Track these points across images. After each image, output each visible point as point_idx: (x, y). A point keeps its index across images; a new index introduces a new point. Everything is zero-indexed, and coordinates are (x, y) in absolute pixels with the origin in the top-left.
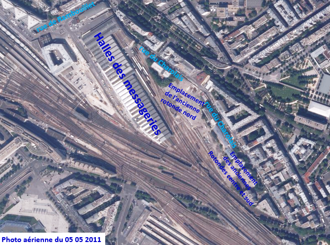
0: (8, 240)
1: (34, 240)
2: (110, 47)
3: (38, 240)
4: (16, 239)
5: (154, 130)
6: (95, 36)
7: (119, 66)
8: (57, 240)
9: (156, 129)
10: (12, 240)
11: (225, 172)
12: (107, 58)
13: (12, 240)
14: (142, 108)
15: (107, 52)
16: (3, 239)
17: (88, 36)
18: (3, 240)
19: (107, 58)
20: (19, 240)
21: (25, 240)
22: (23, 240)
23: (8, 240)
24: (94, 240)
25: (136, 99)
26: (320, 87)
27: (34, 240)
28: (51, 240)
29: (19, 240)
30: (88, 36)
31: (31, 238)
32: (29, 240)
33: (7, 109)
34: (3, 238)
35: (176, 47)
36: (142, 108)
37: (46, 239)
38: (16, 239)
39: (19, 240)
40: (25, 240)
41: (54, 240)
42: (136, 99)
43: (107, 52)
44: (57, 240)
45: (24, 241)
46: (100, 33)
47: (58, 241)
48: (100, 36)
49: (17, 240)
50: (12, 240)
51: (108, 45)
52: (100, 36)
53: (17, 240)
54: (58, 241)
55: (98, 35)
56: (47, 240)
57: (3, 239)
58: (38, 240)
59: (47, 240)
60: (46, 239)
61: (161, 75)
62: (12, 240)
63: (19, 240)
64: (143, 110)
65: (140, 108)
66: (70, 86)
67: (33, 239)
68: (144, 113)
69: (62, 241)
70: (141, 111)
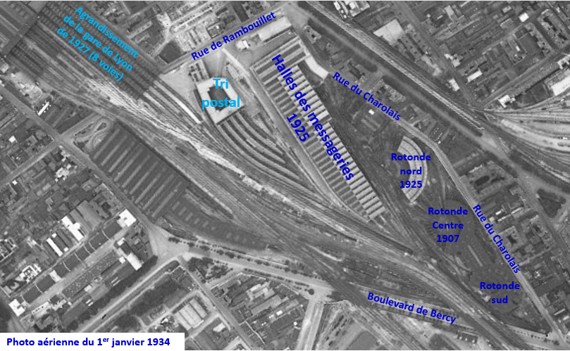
0: (16, 343)
1: (52, 343)
2: (291, 73)
3: (58, 343)
4: (27, 341)
5: (288, 84)
6: (273, 60)
8: (85, 343)
9: (320, 129)
10: (22, 343)
12: (344, 177)
13: (22, 343)
14: (331, 147)
15: (288, 79)
16: (9, 341)
18: (8, 342)
19: (344, 177)
20: (32, 343)
21: (40, 343)
22: (36, 343)
23: (16, 343)
27: (52, 343)
28: (76, 343)
29: (32, 343)
31: (48, 340)
32: (46, 343)
34: (8, 339)
35: (339, 236)
36: (331, 147)
37: (69, 342)
38: (27, 341)
39: (32, 343)
40: (40, 343)
41: (81, 343)
42: (324, 136)
43: (288, 79)
44: (86, 342)
45: (39, 344)
46: (280, 55)
47: (87, 344)
48: (276, 61)
49: (28, 343)
50: (22, 343)
51: (289, 70)
52: (276, 61)
53: (28, 343)
55: (277, 58)
56: (71, 343)
57: (9, 341)
58: (58, 343)
59: (71, 343)
60: (69, 342)
61: (347, 302)
62: (22, 343)
63: (32, 343)
65: (328, 147)
66: (256, 130)
67: (50, 342)
69: (93, 344)
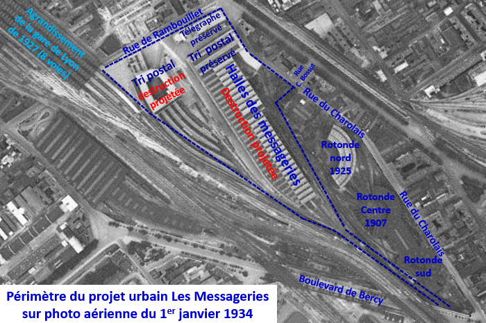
3: (110, 315)
4: (70, 312)
7: (350, 291)
11: (226, 297)
14: (233, 298)
16: (9, 295)
17: (230, 113)
22: (83, 314)
24: (72, 314)
25: (220, 298)
26: (379, 264)
28: (134, 315)
30: (230, 113)
33: (458, 110)
34: (8, 293)
36: (233, 298)
40: (88, 315)
44: (146, 314)
47: (147, 317)
54: (147, 317)
58: (110, 315)
60: (124, 313)
64: (235, 298)
68: (239, 299)
70: (235, 300)
